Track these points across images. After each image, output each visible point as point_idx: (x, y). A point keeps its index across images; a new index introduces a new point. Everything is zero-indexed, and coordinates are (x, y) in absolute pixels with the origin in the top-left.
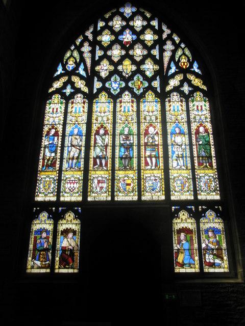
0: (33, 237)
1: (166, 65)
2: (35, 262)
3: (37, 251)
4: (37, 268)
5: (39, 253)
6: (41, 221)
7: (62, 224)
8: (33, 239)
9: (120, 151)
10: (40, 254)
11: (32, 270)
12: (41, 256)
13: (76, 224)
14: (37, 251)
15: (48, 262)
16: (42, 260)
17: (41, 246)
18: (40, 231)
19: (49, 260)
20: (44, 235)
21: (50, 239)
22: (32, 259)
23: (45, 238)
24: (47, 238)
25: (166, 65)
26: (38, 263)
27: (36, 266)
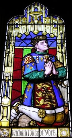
0: (12, 49)
1: (54, 68)
2: (22, 108)
3: (24, 83)
4: (30, 127)
5: (31, 86)
6: (32, 19)
7: (17, 24)
8: (12, 56)
9: (17, 105)
10: (35, 90)
11: (15, 130)
12: (40, 94)
13: (55, 24)
14: (24, 83)
15: (60, 110)
16: (41, 102)
17: (37, 71)
18: (33, 39)
19: (64, 104)
20: (42, 46)
21: (59, 56)
22: (13, 101)
23: (45, 53)
24: (51, 53)
25: (54, 68)
26: (33, 112)
27: (24, 121)
